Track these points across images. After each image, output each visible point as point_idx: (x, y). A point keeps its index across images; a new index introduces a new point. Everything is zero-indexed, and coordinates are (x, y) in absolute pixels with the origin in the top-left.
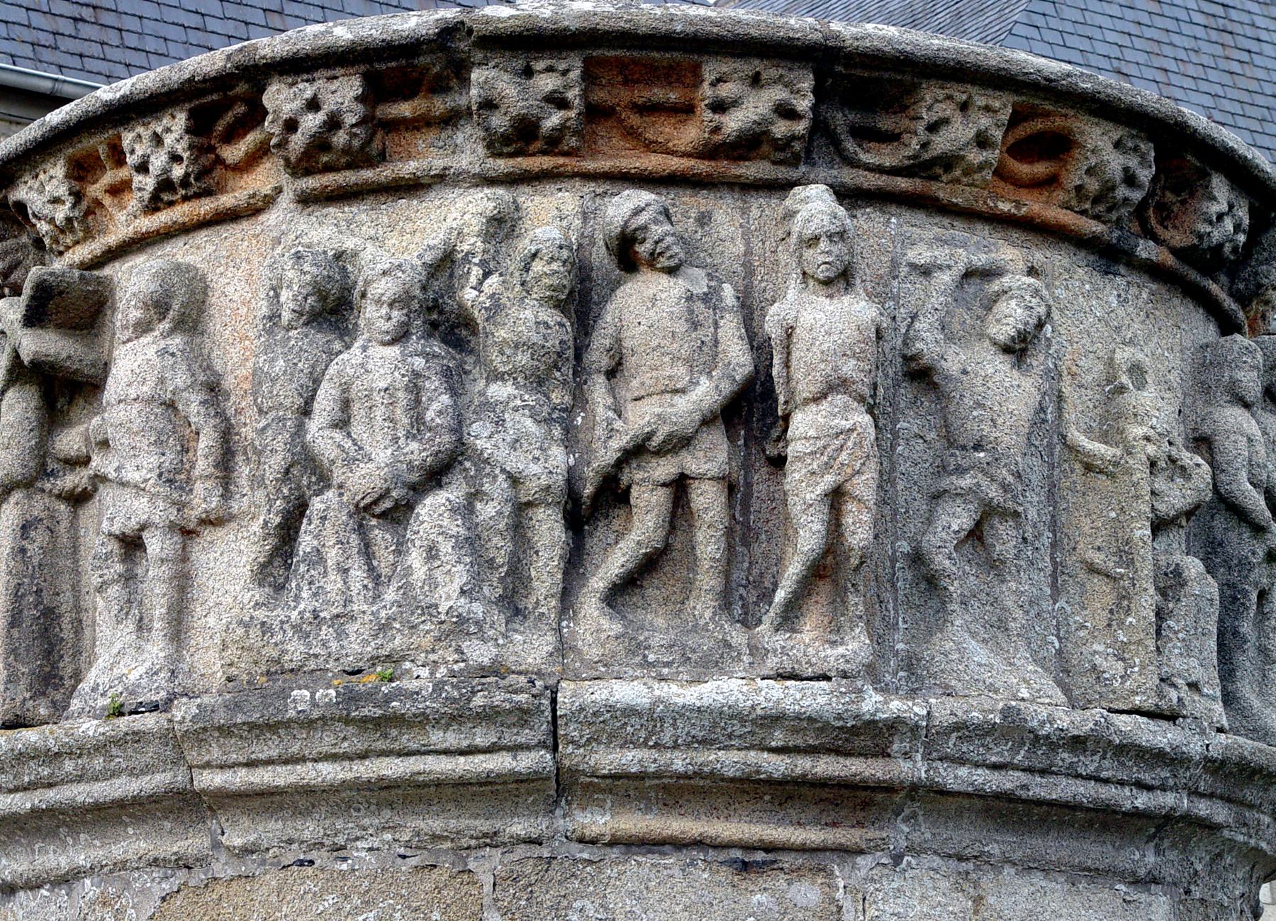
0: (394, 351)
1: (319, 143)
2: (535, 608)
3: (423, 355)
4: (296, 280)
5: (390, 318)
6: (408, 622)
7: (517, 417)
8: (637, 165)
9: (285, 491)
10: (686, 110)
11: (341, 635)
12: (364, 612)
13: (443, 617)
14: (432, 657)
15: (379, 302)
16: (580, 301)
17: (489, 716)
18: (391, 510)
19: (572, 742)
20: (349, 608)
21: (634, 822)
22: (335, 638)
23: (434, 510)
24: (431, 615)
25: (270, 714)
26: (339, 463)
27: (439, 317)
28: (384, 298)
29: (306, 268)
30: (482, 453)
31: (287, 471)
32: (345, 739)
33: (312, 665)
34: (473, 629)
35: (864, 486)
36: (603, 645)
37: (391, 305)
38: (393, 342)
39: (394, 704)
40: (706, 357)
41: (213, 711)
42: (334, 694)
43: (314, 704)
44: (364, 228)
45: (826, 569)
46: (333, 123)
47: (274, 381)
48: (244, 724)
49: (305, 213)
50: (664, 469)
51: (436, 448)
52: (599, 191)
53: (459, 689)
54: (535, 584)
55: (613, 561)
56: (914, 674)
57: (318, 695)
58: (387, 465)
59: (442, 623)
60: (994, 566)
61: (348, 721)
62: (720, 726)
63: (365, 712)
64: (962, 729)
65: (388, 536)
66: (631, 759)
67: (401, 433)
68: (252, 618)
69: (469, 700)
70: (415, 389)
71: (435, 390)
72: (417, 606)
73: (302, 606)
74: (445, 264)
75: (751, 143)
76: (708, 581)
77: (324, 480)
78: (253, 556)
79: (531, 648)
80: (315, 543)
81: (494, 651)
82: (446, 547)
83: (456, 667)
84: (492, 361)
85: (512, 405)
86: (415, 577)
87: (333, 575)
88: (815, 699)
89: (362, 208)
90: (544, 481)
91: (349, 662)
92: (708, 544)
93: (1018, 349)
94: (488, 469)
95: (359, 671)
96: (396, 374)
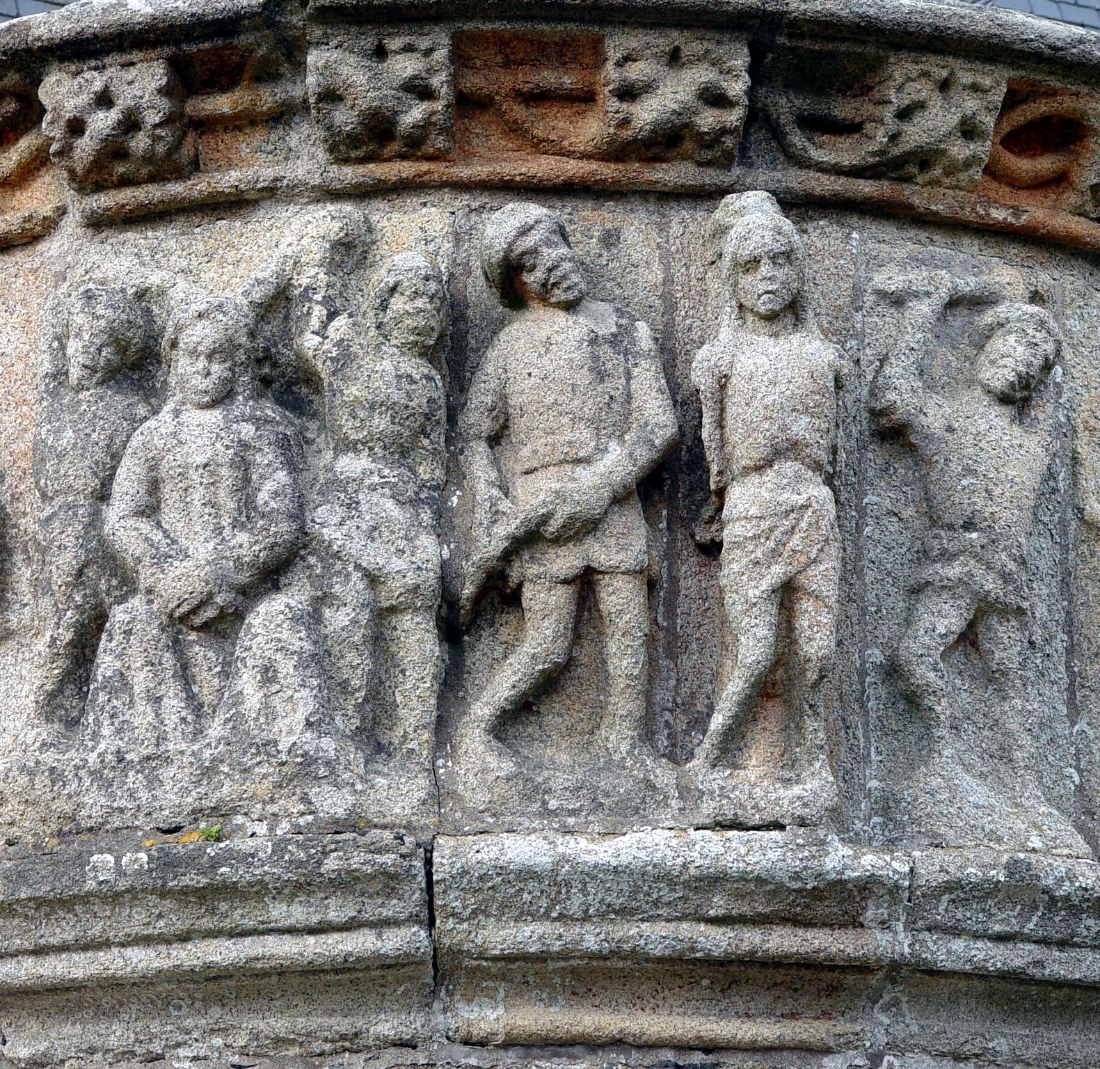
1: (113, 150)
2: (402, 743)
3: (251, 421)
4: (87, 327)
5: (208, 374)
6: (239, 763)
8: (523, 170)
10: (585, 98)
11: (153, 782)
12: (182, 753)
13: (284, 757)
14: (271, 808)
16: (453, 347)
17: (346, 883)
18: (213, 621)
19: (453, 915)
20: (162, 748)
21: (534, 1017)
22: (146, 787)
23: (270, 619)
24: (268, 754)
25: (63, 887)
26: (147, 561)
27: (269, 370)
28: (200, 348)
29: (100, 310)
31: (80, 573)
32: (160, 916)
34: (322, 771)
35: (823, 578)
36: (490, 789)
37: (210, 357)
39: (223, 870)
40: (617, 416)
42: (146, 859)
43: (120, 872)
44: (173, 258)
45: (775, 686)
46: (131, 123)
47: (61, 457)
48: (30, 899)
50: (565, 561)
51: (271, 540)
52: (475, 204)
54: (402, 712)
55: (501, 683)
56: (893, 820)
57: (124, 861)
58: (208, 563)
59: (283, 764)
60: (993, 679)
61: (164, 893)
62: (643, 890)
64: (954, 888)
65: (211, 654)
66: (527, 935)
68: (38, 762)
69: (320, 863)
70: (242, 463)
73: (102, 746)
74: (278, 303)
75: (668, 140)
76: (623, 703)
77: (127, 584)
78: (38, 683)
79: (398, 795)
80: (118, 664)
81: (351, 799)
83: (302, 821)
85: (367, 482)
87: (142, 706)
88: (764, 853)
89: (170, 232)
91: (164, 817)
92: (623, 657)
93: (1019, 398)
96: (218, 445)
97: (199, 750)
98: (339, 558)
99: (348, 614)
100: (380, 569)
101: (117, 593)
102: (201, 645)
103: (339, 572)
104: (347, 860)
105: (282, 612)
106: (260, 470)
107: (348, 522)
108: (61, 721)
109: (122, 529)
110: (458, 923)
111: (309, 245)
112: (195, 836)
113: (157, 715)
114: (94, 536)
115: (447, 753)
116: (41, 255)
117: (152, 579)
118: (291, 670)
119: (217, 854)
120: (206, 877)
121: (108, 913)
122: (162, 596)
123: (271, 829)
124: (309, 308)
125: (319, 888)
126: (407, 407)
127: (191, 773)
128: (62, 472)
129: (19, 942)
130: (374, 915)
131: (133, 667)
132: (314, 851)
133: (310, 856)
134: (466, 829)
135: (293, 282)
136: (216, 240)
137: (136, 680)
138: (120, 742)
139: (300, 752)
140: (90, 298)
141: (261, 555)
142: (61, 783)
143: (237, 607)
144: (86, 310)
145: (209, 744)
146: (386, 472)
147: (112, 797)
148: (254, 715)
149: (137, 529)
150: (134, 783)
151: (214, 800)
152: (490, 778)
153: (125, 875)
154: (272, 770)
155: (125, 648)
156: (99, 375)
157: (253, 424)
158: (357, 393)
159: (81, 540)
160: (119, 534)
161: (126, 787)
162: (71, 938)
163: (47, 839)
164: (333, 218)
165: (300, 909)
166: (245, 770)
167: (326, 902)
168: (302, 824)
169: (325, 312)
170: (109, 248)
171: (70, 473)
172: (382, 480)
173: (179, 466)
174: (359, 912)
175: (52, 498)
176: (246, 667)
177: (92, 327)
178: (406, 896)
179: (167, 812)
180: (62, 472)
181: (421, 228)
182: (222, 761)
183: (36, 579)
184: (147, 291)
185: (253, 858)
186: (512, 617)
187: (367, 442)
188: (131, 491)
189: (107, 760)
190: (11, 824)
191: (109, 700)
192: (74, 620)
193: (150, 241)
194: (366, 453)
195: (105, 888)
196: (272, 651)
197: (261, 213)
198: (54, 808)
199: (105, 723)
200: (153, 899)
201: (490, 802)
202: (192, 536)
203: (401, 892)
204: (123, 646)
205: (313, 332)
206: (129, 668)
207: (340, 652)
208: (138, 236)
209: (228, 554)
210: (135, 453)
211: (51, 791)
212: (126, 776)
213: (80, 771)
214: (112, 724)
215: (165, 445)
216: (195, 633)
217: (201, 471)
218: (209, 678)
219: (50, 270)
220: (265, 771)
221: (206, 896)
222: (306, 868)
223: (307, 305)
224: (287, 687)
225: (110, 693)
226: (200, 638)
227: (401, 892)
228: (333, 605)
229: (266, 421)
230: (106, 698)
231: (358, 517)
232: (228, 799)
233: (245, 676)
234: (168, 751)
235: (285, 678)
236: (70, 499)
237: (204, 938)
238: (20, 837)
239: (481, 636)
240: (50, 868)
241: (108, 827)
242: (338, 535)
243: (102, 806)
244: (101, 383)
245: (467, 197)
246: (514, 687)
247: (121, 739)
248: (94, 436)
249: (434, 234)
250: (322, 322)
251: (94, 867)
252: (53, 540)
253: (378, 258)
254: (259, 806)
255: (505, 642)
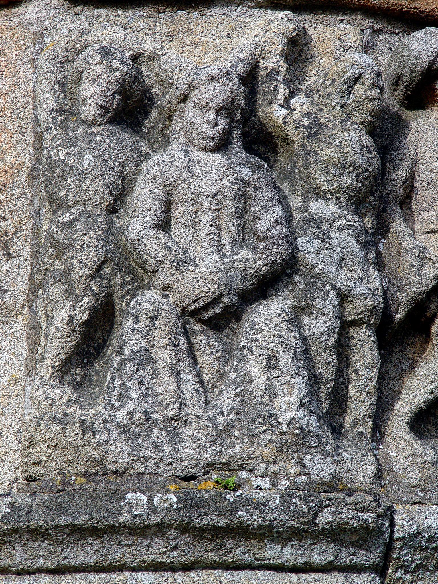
0: (218, 158)
2: (353, 427)
3: (240, 164)
4: (104, 76)
5: (216, 125)
6: (248, 430)
7: (343, 235)
8: (417, 5)
9: (95, 288)
11: (174, 439)
12: (199, 417)
13: (285, 429)
14: (273, 468)
15: (205, 107)
17: (336, 534)
18: (219, 316)
19: (402, 567)
20: (183, 412)
22: (169, 442)
24: (272, 425)
25: (100, 517)
26: (167, 264)
27: (248, 132)
28: (211, 104)
29: (115, 64)
30: (312, 268)
31: (99, 268)
32: (175, 548)
33: (140, 468)
34: (314, 442)
36: (420, 469)
37: (217, 112)
38: (215, 150)
39: (240, 513)
41: (29, 511)
42: (175, 499)
43: (152, 509)
44: (140, 34)
47: (83, 175)
48: (68, 526)
49: (72, 11)
51: (273, 258)
52: (377, 26)
53: (307, 502)
54: (353, 403)
57: (156, 499)
58: (220, 271)
59: (283, 433)
61: (184, 529)
63: (208, 520)
65: (213, 342)
67: (226, 240)
68: (66, 415)
69: (316, 515)
71: (269, 200)
72: (255, 414)
73: (131, 406)
78: (55, 352)
80: (144, 342)
81: (333, 467)
82: (285, 358)
83: (299, 480)
84: (314, 178)
85: (337, 223)
86: (254, 385)
87: (166, 378)
89: (137, 13)
90: (370, 303)
91: (182, 467)
94: (318, 285)
95: (193, 478)
96: (225, 181)
97: (213, 416)
98: (319, 279)
99: (326, 323)
100: (350, 291)
101: (130, 287)
102: (205, 335)
103: (320, 289)
104: (339, 514)
105: (280, 315)
106: (262, 204)
107: (322, 252)
108: (69, 384)
109: (146, 237)
110: (404, 574)
111: (272, 37)
112: (210, 485)
113: (178, 386)
114: (112, 240)
115: (377, 438)
116: (18, 16)
117: (172, 279)
118: (290, 360)
119: (234, 500)
120: (226, 518)
121: (130, 542)
122: (180, 292)
123: (274, 485)
124: (276, 86)
125: (311, 535)
126: (367, 170)
127: (208, 434)
128: (84, 187)
129: (42, 561)
130: (346, 561)
131: (157, 345)
132: (313, 505)
133: (310, 509)
134: (405, 499)
135: (260, 64)
136: (177, 25)
137: (160, 356)
138: (146, 405)
139: (297, 425)
140: (106, 53)
141: (264, 269)
142: (91, 433)
143: (238, 308)
144: (105, 62)
145: (221, 413)
146: (350, 217)
147: (138, 447)
148: (261, 393)
149: (157, 238)
150: (158, 438)
151: (227, 457)
152: (420, 461)
153: (157, 511)
154: (275, 437)
155: (150, 330)
156: (110, 115)
157: (249, 167)
158: (331, 154)
159: (101, 242)
160: (143, 240)
161: (150, 441)
162: (92, 560)
163: (74, 478)
164: (289, 20)
165: (291, 551)
166: (253, 435)
167: (312, 547)
168: (299, 482)
169: (287, 91)
170: (83, 19)
171: (91, 188)
172: (347, 223)
173: (192, 193)
174: (336, 558)
175: (71, 207)
176: (252, 354)
177: (109, 77)
178: (373, 548)
179: (186, 464)
180: (84, 187)
181: (339, 39)
182: (233, 427)
183: (46, 270)
184: (140, 55)
185: (265, 506)
186: (417, 340)
187: (336, 193)
188: (154, 208)
189: (135, 418)
190: (37, 463)
191: (137, 370)
192: (90, 304)
193: (121, 19)
194: (334, 201)
195: (138, 521)
196: (274, 344)
197: (215, 10)
198: (84, 452)
199: (133, 388)
200: (173, 533)
201: (421, 480)
202: (198, 249)
203: (370, 544)
204: (148, 328)
205: (280, 105)
206: (153, 346)
207: (317, 351)
208: (110, 13)
209: (236, 265)
210: (154, 179)
211: (83, 438)
212: (151, 432)
213: (108, 425)
214: (140, 389)
215: (181, 175)
216: (199, 324)
217: (210, 199)
218: (210, 361)
219: (28, 29)
220: (269, 437)
221: (215, 533)
222: (306, 518)
223: (274, 83)
224: (286, 374)
225: (138, 364)
226: (203, 329)
227: (370, 544)
228: (312, 314)
229: (259, 167)
230: (135, 368)
231: (331, 249)
232: (239, 457)
233: (251, 362)
234: (188, 415)
235: (285, 366)
236: (89, 209)
237: (204, 569)
238: (43, 474)
239: (393, 351)
240: (89, 502)
241: (132, 471)
242: (316, 261)
243: (129, 454)
244: (109, 122)
245: (372, 21)
246: (431, 393)
247: (146, 402)
248: (110, 162)
249: (350, 44)
250: (286, 98)
251: (129, 503)
252: (75, 240)
253: (309, 56)
254: (263, 465)
255: (411, 358)
